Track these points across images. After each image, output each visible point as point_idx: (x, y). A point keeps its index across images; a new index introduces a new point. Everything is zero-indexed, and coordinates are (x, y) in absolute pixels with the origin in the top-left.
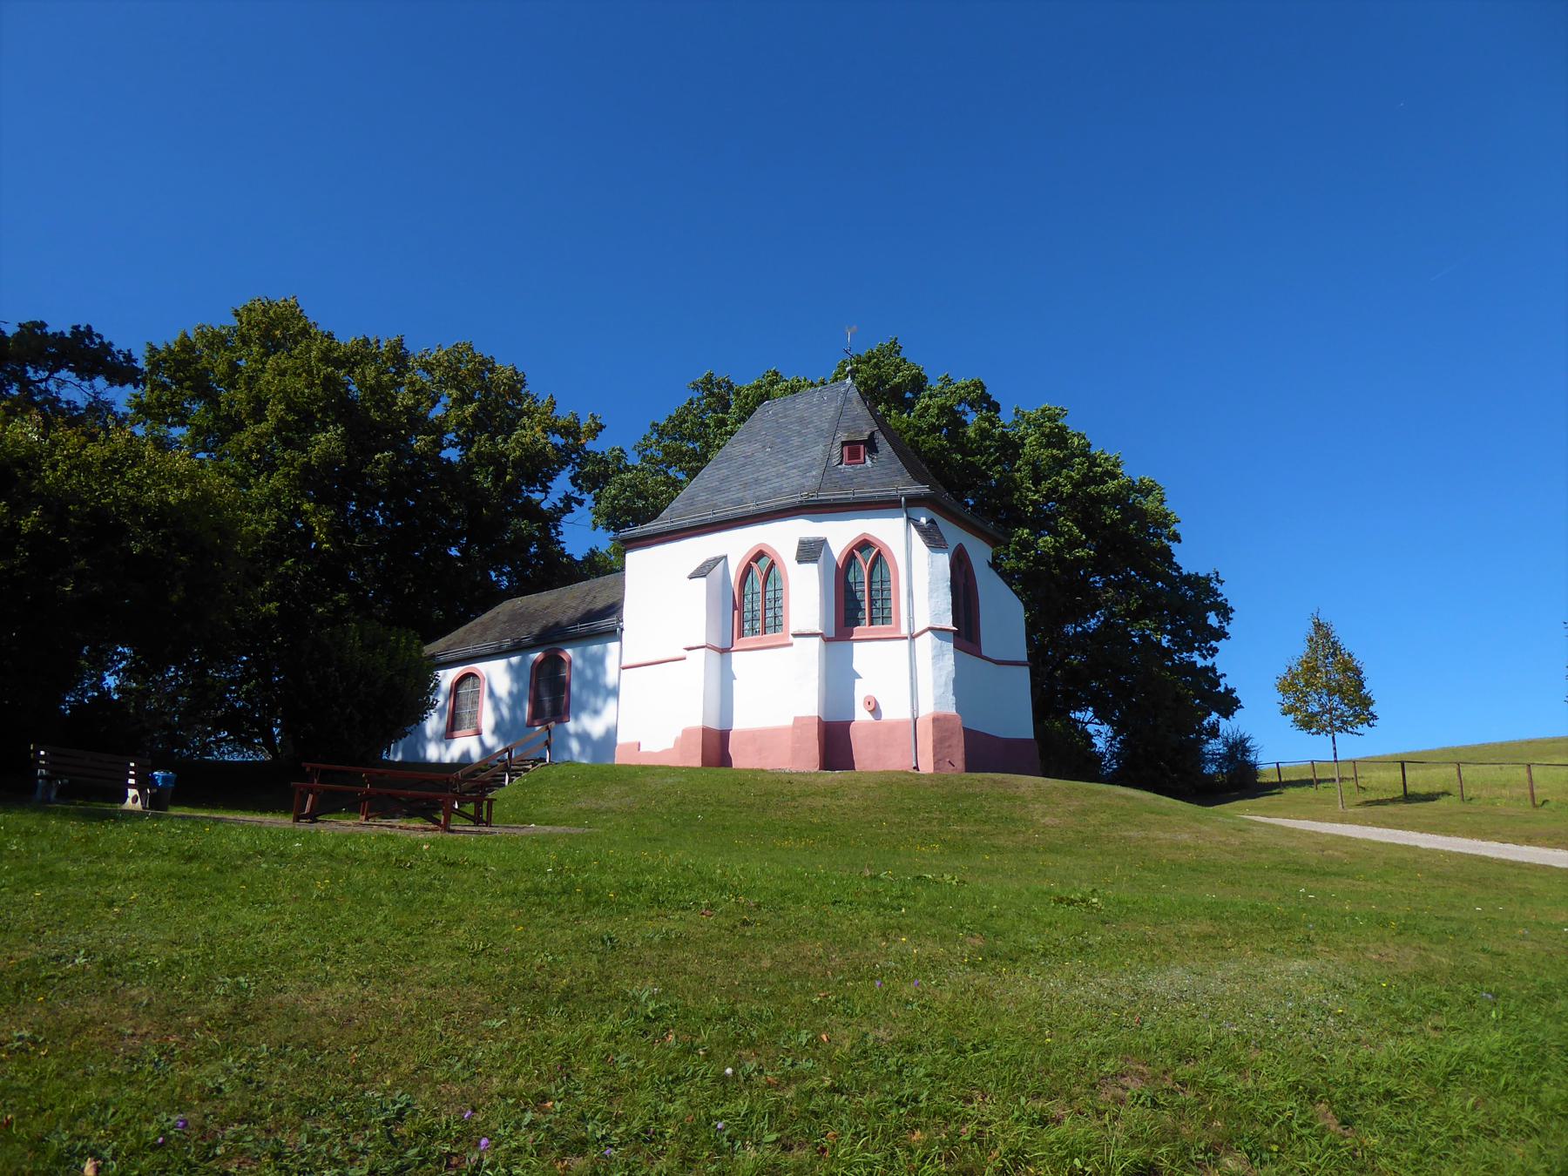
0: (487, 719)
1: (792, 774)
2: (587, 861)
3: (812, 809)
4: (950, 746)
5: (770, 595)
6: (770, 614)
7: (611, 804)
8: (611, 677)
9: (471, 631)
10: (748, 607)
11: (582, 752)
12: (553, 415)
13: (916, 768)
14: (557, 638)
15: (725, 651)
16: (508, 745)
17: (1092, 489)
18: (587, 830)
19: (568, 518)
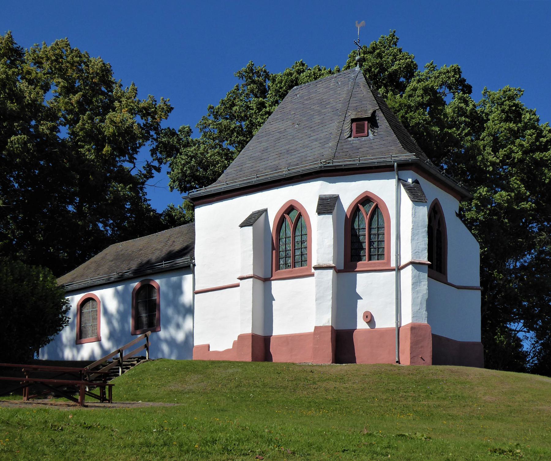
0: (104, 330)
1: (313, 366)
2: (178, 424)
3: (327, 390)
4: (422, 347)
5: (298, 239)
6: (298, 253)
7: (191, 387)
8: (187, 297)
9: (88, 268)
10: (282, 248)
11: (171, 353)
12: (137, 99)
13: (398, 362)
14: (149, 271)
15: (267, 280)
16: (120, 348)
17: (537, 155)
18: (176, 405)
19: (150, 182)
